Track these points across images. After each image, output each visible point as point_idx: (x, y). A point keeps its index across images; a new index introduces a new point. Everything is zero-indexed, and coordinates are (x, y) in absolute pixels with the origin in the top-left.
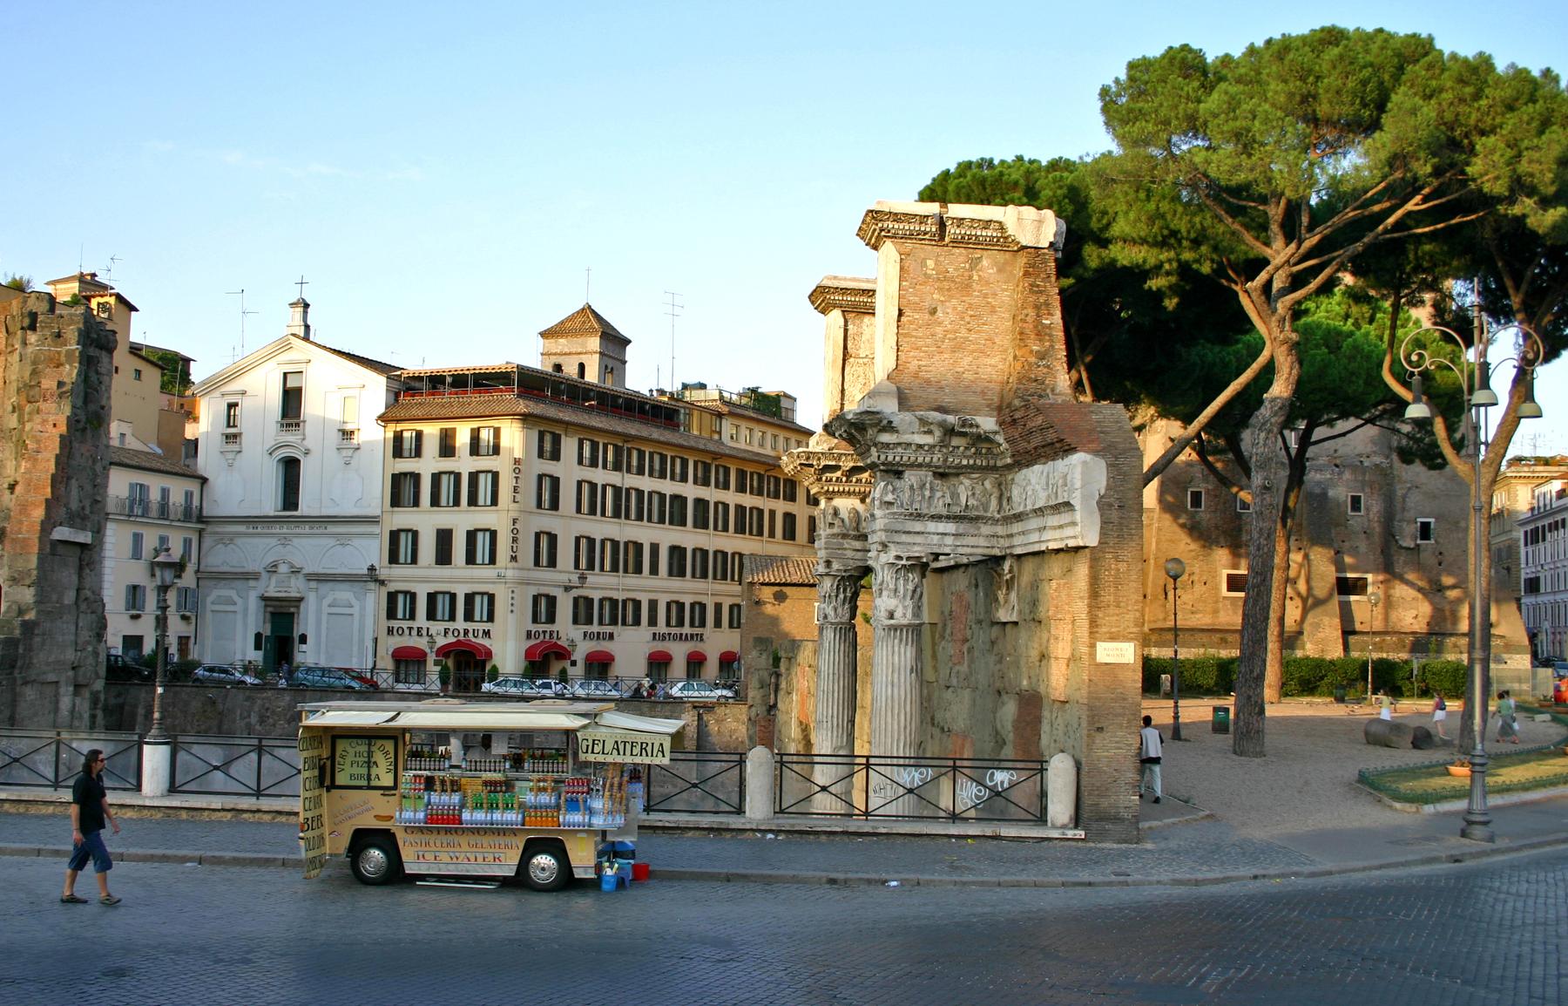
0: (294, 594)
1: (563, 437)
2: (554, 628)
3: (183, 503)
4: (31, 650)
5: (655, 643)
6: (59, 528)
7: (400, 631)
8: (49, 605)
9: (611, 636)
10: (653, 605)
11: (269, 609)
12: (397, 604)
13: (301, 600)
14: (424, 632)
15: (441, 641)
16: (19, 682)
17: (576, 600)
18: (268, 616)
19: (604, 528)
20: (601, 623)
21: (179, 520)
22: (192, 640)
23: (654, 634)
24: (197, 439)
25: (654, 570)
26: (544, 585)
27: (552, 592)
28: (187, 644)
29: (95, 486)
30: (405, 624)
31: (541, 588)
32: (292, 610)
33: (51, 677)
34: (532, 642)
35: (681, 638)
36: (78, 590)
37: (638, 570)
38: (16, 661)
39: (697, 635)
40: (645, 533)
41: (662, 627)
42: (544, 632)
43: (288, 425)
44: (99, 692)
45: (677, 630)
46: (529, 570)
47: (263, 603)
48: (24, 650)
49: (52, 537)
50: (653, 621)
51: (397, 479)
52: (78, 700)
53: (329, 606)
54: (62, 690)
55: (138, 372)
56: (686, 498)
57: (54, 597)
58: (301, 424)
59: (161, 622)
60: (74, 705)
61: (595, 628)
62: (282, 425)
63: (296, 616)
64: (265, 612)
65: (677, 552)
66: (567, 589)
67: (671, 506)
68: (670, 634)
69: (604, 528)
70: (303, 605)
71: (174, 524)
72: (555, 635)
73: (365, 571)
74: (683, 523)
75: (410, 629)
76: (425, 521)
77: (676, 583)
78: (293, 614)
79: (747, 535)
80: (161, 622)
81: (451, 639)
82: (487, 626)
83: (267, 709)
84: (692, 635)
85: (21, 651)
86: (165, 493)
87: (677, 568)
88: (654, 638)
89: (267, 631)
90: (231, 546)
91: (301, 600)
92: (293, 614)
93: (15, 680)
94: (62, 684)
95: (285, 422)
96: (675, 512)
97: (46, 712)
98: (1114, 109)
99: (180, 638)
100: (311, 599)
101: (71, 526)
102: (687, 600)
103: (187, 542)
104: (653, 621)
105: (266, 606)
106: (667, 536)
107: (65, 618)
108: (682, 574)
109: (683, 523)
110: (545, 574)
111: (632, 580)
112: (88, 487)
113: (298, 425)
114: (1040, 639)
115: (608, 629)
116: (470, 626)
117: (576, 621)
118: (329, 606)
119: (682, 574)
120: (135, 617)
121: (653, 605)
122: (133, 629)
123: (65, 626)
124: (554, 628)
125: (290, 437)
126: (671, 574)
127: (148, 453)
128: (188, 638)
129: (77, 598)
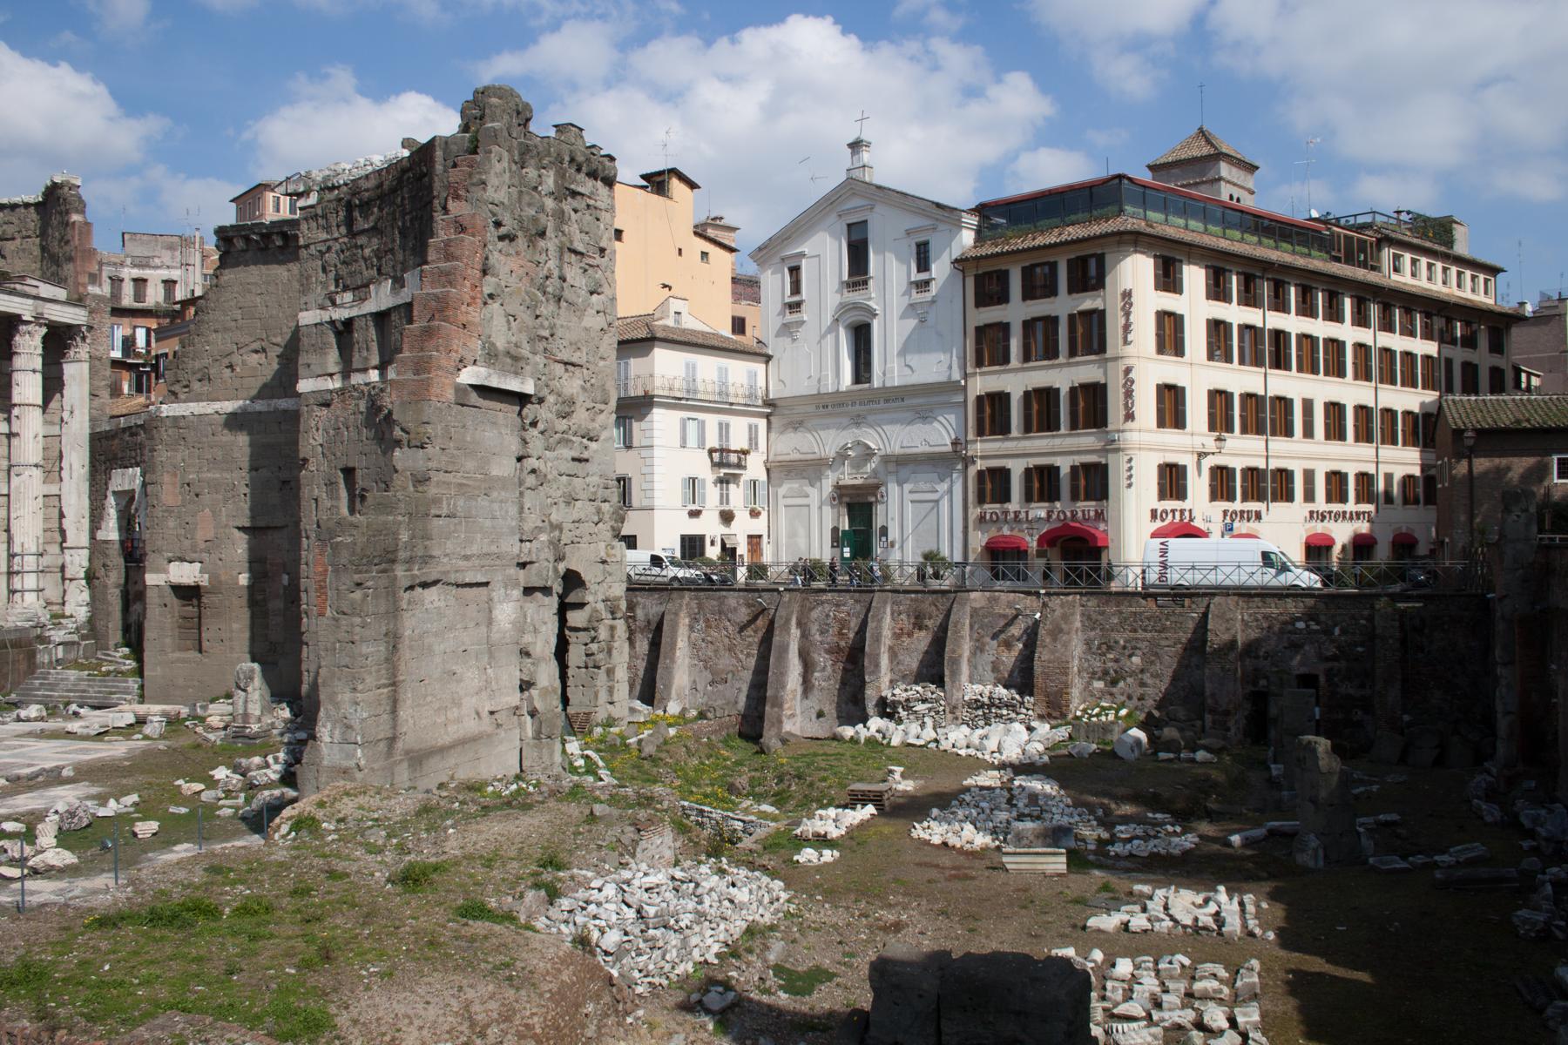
2: (1186, 505)
5: (1313, 523)
7: (996, 521)
9: (1258, 516)
10: (1309, 476)
11: (846, 499)
12: (994, 484)
19: (1241, 379)
22: (765, 539)
23: (1311, 513)
25: (1308, 432)
27: (1181, 460)
28: (759, 544)
31: (1167, 455)
35: (1344, 517)
37: (1288, 432)
39: (1364, 513)
40: (1289, 384)
41: (1320, 503)
42: (1173, 511)
44: (619, 599)
45: (1336, 507)
46: (1150, 431)
49: (459, 380)
50: (1309, 496)
55: (704, 255)
56: (1344, 343)
61: (1238, 505)
65: (1335, 411)
66: (1202, 455)
67: (1326, 353)
68: (1330, 512)
69: (1241, 379)
72: (1187, 514)
73: (949, 448)
74: (1341, 373)
76: (1016, 381)
77: (1335, 447)
78: (870, 504)
79: (1419, 389)
84: (1358, 514)
87: (1335, 431)
88: (1311, 517)
92: (870, 504)
96: (1331, 359)
99: (750, 537)
102: (1351, 470)
103: (753, 430)
104: (1309, 496)
106: (1319, 389)
108: (1341, 436)
109: (1341, 373)
110: (1171, 436)
111: (1279, 444)
113: (865, 283)
114: (840, 634)
115: (1253, 506)
119: (1341, 436)
120: (695, 514)
121: (1309, 476)
122: (693, 528)
124: (1186, 505)
125: (856, 297)
126: (1328, 437)
128: (760, 537)
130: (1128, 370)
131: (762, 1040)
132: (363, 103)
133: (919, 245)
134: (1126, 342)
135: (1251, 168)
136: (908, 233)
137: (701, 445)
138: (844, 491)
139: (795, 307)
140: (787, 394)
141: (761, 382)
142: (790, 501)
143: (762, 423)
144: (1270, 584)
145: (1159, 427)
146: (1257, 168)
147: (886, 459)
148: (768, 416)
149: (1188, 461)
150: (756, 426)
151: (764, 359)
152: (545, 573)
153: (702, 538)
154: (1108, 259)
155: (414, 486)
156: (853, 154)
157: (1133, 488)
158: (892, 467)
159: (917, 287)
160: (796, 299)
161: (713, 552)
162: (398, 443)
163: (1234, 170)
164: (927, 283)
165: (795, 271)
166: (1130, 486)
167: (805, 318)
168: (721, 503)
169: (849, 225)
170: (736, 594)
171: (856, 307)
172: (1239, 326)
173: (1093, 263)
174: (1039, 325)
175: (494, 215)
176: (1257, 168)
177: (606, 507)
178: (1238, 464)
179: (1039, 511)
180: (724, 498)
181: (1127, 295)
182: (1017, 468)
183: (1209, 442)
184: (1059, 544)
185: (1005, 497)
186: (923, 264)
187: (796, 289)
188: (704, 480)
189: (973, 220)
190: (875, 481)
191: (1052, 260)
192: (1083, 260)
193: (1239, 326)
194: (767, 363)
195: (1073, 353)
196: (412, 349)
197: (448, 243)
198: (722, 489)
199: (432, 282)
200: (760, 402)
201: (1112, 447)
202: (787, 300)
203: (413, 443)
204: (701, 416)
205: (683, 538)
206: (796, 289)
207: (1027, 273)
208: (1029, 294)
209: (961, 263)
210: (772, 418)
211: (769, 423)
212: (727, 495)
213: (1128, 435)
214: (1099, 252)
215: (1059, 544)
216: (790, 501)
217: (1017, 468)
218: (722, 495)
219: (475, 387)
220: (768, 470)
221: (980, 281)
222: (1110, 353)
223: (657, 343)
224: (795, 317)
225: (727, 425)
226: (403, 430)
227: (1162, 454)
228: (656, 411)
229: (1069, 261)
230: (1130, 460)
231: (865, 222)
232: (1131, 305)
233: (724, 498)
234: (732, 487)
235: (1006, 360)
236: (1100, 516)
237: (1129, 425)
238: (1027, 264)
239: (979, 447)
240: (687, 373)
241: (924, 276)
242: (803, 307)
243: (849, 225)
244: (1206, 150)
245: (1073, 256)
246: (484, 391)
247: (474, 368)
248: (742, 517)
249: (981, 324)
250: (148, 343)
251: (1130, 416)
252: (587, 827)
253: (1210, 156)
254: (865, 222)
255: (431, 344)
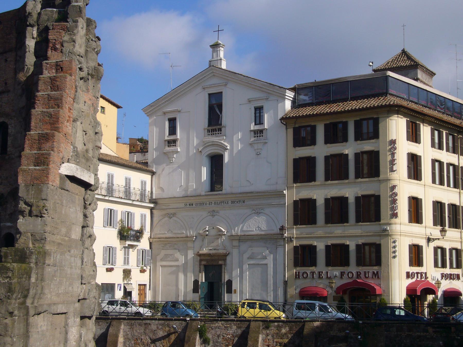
0: (221, 251)
1: (421, 125)
3: (140, 188)
4: (42, 280)
6: (66, 164)
7: (305, 276)
8: (58, 237)
11: (204, 263)
13: (226, 255)
14: (324, 275)
15: (337, 283)
16: (32, 312)
17: (436, 249)
18: (202, 267)
20: (451, 267)
21: (138, 201)
24: (210, 46)
26: (416, 237)
29: (96, 133)
30: (309, 270)
31: (414, 239)
32: (220, 262)
33: (61, 308)
34: (410, 281)
36: (83, 227)
38: (28, 290)
43: (213, 130)
46: (405, 225)
47: (199, 258)
48: (37, 279)
51: (297, 162)
52: (83, 332)
53: (248, 258)
54: (71, 321)
57: (64, 230)
58: (223, 129)
59: (127, 273)
60: (81, 336)
61: (448, 271)
62: (209, 131)
63: (223, 266)
64: (200, 265)
70: (228, 258)
71: (134, 203)
75: (313, 273)
78: (221, 265)
80: (127, 273)
81: (345, 281)
82: (375, 269)
83: (219, 336)
85: (33, 280)
86: (128, 181)
89: (202, 278)
90: (174, 218)
91: (226, 255)
92: (221, 265)
93: (27, 309)
94: (71, 315)
95: (210, 128)
97: (57, 343)
98: (102, 284)
100: (235, 252)
101: (77, 163)
103: (143, 217)
105: (201, 261)
107: (72, 251)
110: (415, 228)
112: (91, 132)
113: (220, 130)
116: (362, 269)
117: (436, 265)
118: (248, 258)
120: (109, 270)
123: (73, 259)
125: (215, 139)
127: (116, 157)
128: (145, 285)
129: (82, 235)
130: (394, 187)
133: (256, 109)
134: (392, 170)
135: (432, 74)
136: (250, 101)
138: (203, 258)
139: (173, 143)
140: (165, 196)
141: (148, 188)
142: (164, 263)
143: (147, 212)
144: (258, 316)
145: (410, 221)
146: (435, 74)
147: (232, 238)
149: (422, 243)
150: (145, 215)
151: (151, 174)
152: (93, 306)
154: (380, 120)
155: (33, 244)
156: (213, 52)
157: (397, 259)
158: (236, 243)
159: (255, 133)
160: (172, 137)
161: (119, 295)
162: (22, 213)
163: (424, 75)
164: (174, 141)
165: (173, 122)
166: (394, 257)
167: (179, 150)
168: (125, 263)
169: (210, 95)
170: (157, 321)
171: (214, 144)
172: (447, 163)
173: (340, 126)
174: (365, 157)
175: (80, 63)
176: (435, 74)
178: (447, 246)
179: (336, 271)
180: (126, 261)
181: (393, 142)
182: (321, 246)
183: (436, 232)
184: (348, 292)
185: (314, 263)
186: (259, 120)
187: (173, 131)
188: (116, 248)
189: (290, 95)
190: (224, 252)
191: (313, 124)
192: (335, 125)
193: (447, 163)
195: (357, 176)
196: (31, 147)
197: (53, 80)
199: (43, 104)
201: (385, 234)
202: (166, 138)
203: (35, 213)
206: (173, 131)
207: (358, 125)
208: (329, 140)
209: (286, 120)
211: (152, 213)
212: (128, 258)
213: (394, 227)
214: (375, 116)
215: (348, 292)
216: (164, 263)
217: (321, 246)
218: (125, 258)
219: (68, 176)
220: (151, 244)
221: (296, 132)
222: (382, 177)
224: (172, 148)
226: (26, 203)
227: (411, 239)
229: (325, 125)
230: (394, 242)
231: (222, 92)
232: (395, 149)
233: (126, 261)
235: (347, 177)
236: (376, 275)
237: (394, 220)
238: (358, 119)
239: (294, 232)
240: (109, 180)
241: (172, 137)
242: (178, 143)
243: (210, 95)
244: (408, 63)
245: (328, 122)
246: (73, 179)
247: (68, 164)
248: (135, 273)
249: (297, 157)
251: (395, 215)
253: (411, 65)
254: (222, 92)
255: (47, 145)
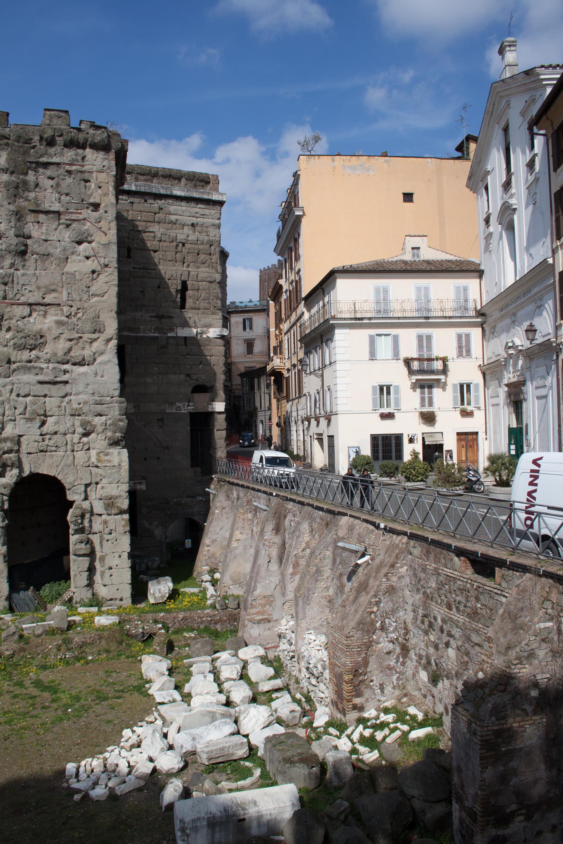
22: (481, 436)
128: (477, 433)
131: (2, 292)
132: (332, 345)
137: (396, 355)
148: (482, 325)
150: (468, 336)
151: (477, 274)
153: (399, 438)
177: (512, 607)
194: (481, 277)
198: (422, 393)
200: (473, 313)
204: (394, 331)
205: (375, 438)
210: (484, 326)
220: (484, 374)
223: (337, 275)
225: (429, 338)
228: (337, 331)
234: (436, 391)
250: (108, 613)
252: (46, 365)
